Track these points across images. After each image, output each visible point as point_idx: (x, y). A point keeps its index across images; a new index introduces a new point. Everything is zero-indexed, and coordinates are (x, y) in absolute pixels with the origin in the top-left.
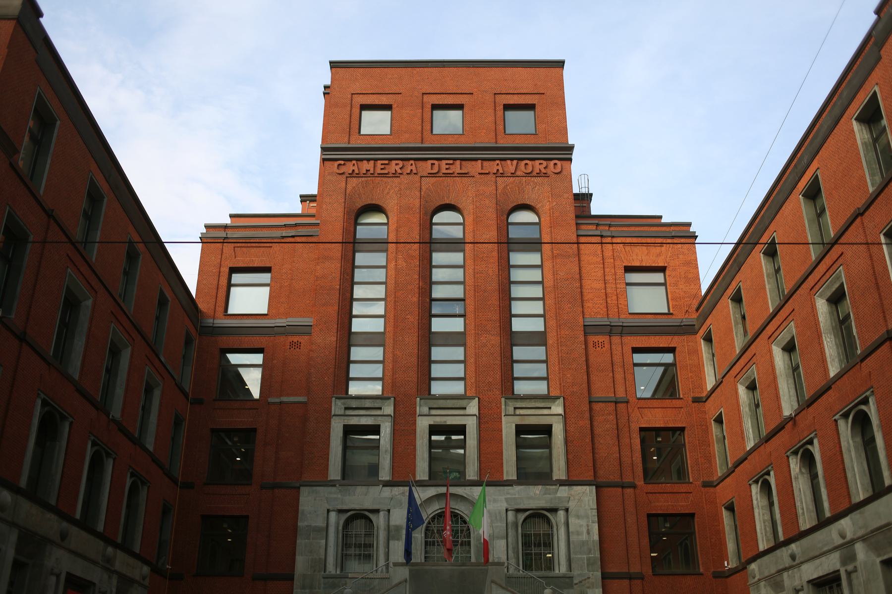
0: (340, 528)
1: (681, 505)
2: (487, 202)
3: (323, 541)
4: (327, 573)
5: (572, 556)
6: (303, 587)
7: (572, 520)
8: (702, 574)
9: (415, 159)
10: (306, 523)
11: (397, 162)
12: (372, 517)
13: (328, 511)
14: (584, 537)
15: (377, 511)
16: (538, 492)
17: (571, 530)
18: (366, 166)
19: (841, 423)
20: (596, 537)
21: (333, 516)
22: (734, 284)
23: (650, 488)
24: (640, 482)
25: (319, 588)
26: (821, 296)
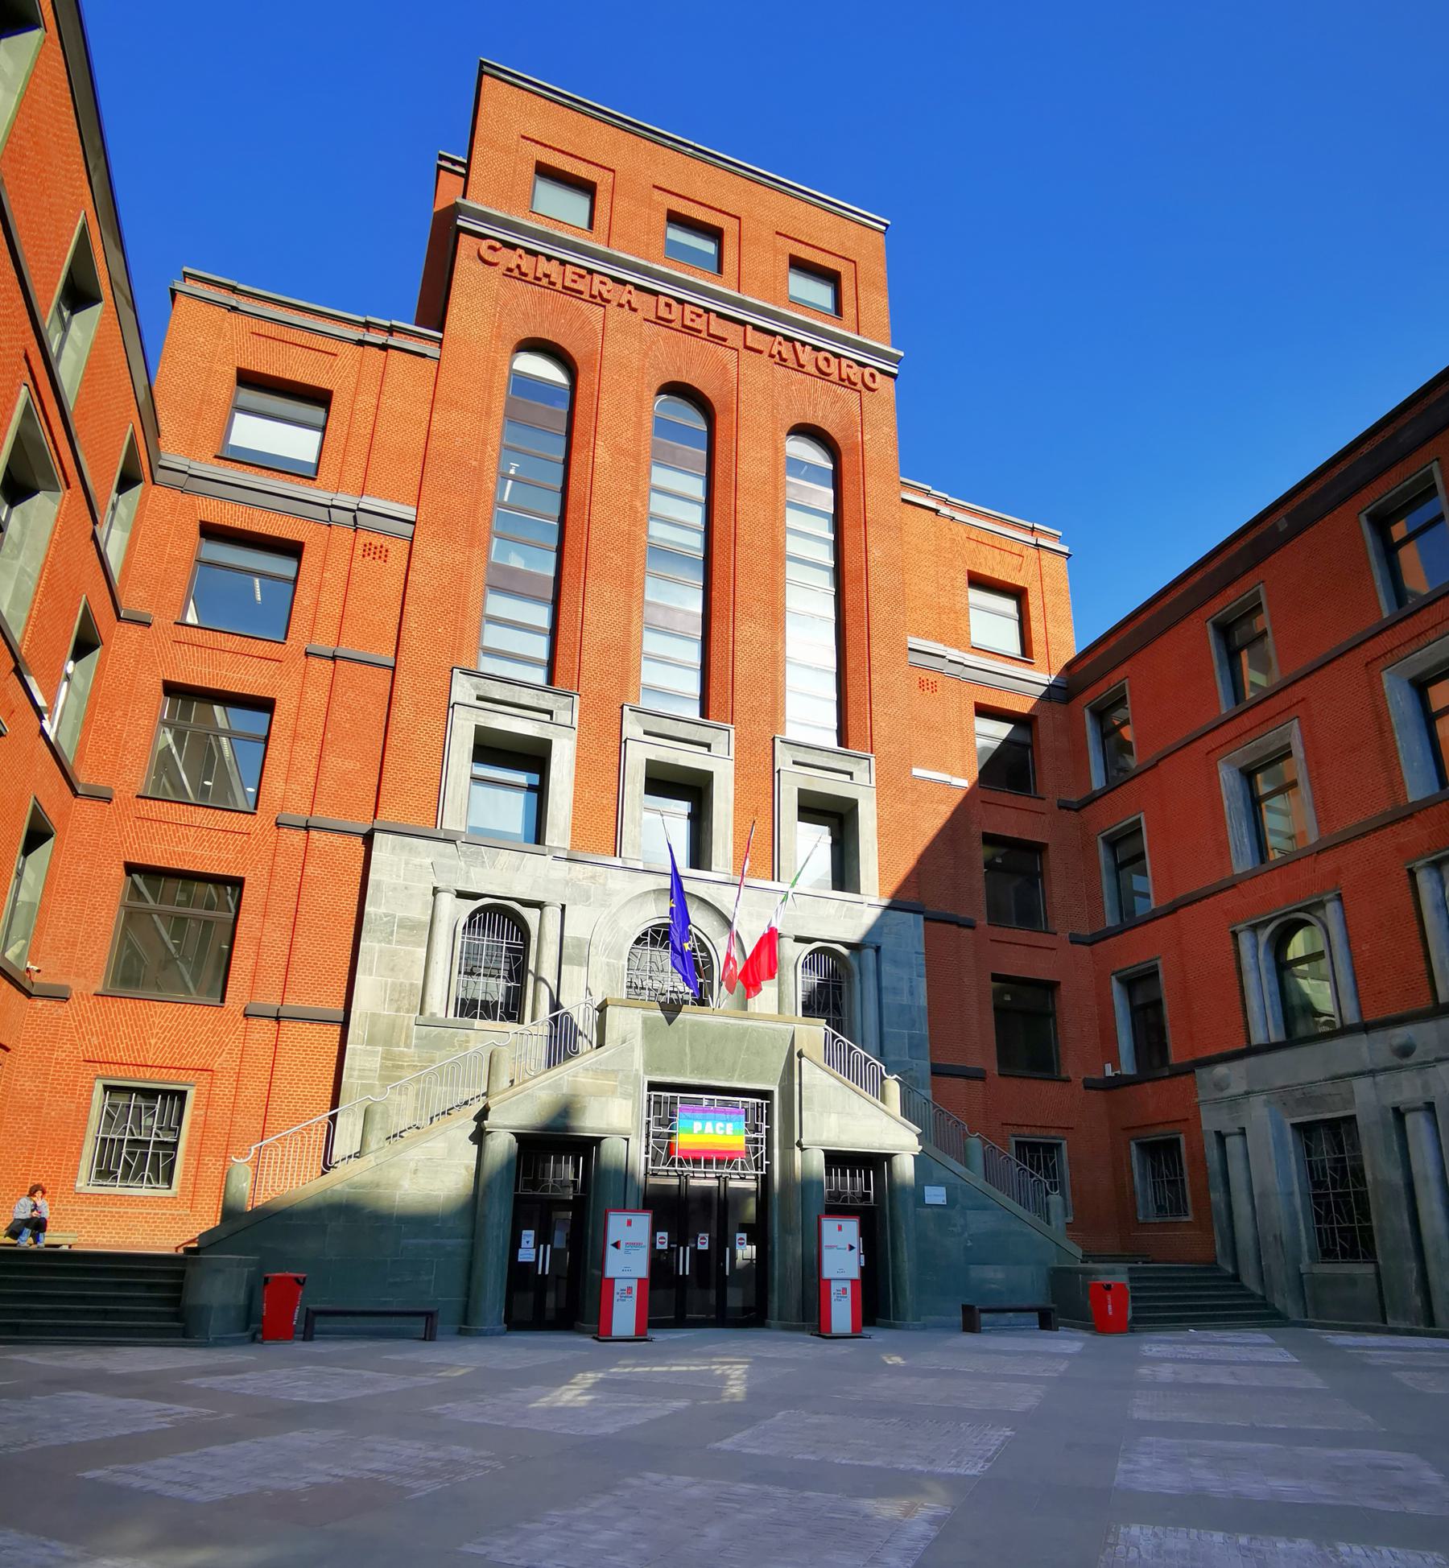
0: (460, 929)
1: (1039, 968)
2: (759, 398)
3: (422, 952)
4: (427, 1013)
5: (886, 1029)
6: (371, 1041)
7: (886, 968)
8: (1068, 1080)
9: (638, 287)
10: (382, 910)
11: (605, 279)
12: (531, 916)
13: (435, 891)
14: (905, 1000)
15: (539, 905)
16: (832, 911)
17: (884, 983)
18: (544, 266)
19: (1245, 940)
20: (923, 1001)
21: (447, 901)
22: (1116, 676)
23: (997, 932)
24: (982, 922)
25: (407, 1046)
26: (1228, 762)
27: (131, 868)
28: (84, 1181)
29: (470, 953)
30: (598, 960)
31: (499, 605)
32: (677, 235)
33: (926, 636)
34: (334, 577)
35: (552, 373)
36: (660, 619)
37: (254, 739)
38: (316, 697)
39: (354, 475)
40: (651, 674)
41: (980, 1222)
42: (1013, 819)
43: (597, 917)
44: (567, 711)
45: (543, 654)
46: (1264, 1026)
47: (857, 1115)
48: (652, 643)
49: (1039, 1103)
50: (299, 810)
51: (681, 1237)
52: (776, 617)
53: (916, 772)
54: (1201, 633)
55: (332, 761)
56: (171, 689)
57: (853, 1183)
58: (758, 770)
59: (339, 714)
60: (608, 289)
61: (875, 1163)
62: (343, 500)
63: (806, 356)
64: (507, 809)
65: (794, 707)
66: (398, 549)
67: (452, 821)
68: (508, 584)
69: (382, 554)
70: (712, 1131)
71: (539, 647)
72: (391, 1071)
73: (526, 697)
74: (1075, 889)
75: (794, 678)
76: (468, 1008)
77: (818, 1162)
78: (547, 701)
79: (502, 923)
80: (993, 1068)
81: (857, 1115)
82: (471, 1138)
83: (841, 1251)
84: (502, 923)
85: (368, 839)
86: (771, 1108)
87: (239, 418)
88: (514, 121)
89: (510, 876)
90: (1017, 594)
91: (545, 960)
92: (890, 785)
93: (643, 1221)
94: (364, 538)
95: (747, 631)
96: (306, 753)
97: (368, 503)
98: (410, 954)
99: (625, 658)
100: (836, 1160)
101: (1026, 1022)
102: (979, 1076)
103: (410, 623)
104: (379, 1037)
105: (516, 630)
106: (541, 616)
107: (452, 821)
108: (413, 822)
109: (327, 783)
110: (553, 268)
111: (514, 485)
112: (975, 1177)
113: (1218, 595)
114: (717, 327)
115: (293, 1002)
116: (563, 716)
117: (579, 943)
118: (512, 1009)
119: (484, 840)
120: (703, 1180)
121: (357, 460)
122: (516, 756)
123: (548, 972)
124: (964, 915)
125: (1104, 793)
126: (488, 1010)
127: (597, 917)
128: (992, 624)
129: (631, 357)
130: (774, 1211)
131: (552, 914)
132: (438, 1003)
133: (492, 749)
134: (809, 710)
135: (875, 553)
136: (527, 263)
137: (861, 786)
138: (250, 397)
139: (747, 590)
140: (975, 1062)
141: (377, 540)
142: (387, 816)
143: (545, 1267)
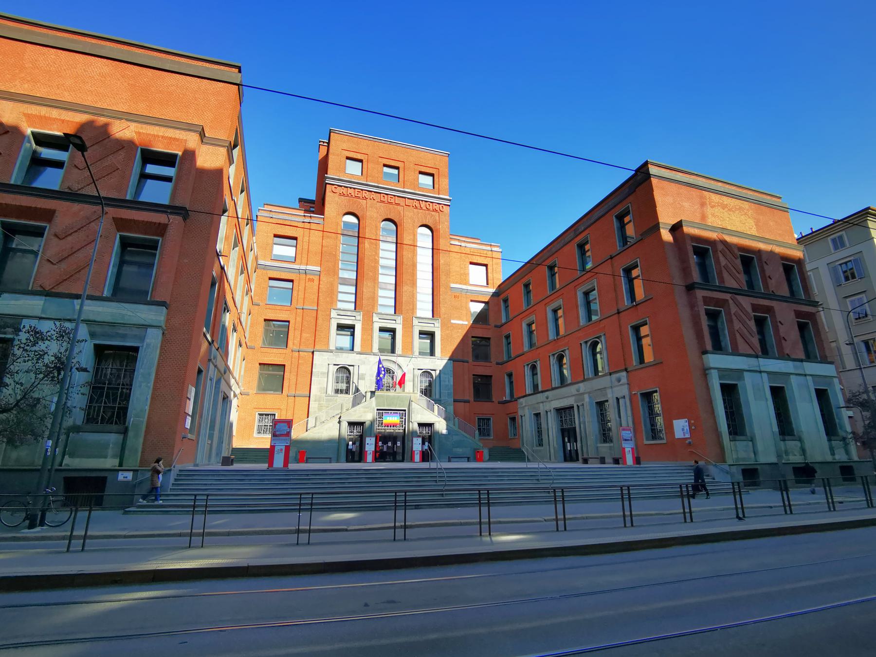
12: (351, 368)
18: (350, 191)
23: (476, 363)
24: (471, 361)
27: (260, 364)
28: (255, 435)
29: (337, 378)
30: (367, 378)
31: (342, 288)
32: (386, 169)
33: (456, 283)
34: (302, 288)
35: (354, 220)
36: (383, 286)
37: (411, 527)
38: (299, 319)
39: (304, 260)
40: (381, 301)
41: (455, 438)
42: (480, 333)
43: (365, 372)
44: (359, 316)
45: (354, 300)
46: (556, 382)
47: (427, 414)
48: (381, 293)
49: (485, 408)
50: (296, 348)
51: (385, 442)
52: (414, 283)
53: (453, 321)
54: (573, 248)
55: (304, 335)
56: (265, 320)
57: (425, 431)
58: (408, 326)
59: (305, 323)
60: (367, 195)
61: (430, 425)
62: (303, 267)
63: (423, 204)
64: (344, 340)
65: (419, 305)
66: (316, 278)
67: (332, 347)
68: (345, 282)
69: (312, 280)
70: (389, 419)
71: (352, 298)
72: (320, 408)
73: (349, 313)
74: (497, 351)
75: (419, 297)
76: (337, 391)
77: (416, 427)
78: (354, 314)
79: (345, 370)
80: (472, 399)
81: (427, 414)
82: (422, 392)
83: (417, 445)
84: (345, 370)
85: (313, 353)
86: (404, 413)
87: (275, 246)
88: (340, 144)
89: (345, 359)
90: (486, 265)
91: (354, 378)
92: (445, 326)
93: (373, 439)
94: (308, 277)
95: (405, 289)
96: (298, 333)
97: (309, 267)
98: (324, 380)
99: (374, 298)
100: (420, 425)
101: (482, 387)
102: (468, 402)
103: (321, 298)
104: (318, 400)
105: (346, 295)
106: (352, 289)
107: (332, 347)
108: (324, 348)
109: (303, 340)
110: (351, 191)
111: (346, 248)
112: (456, 428)
113: (545, 261)
114: (398, 200)
115: (298, 393)
116: (358, 318)
117: (363, 375)
118: (347, 391)
119: (340, 349)
120: (390, 430)
121: (305, 256)
122: (347, 328)
123: (355, 381)
124: (466, 359)
125: (506, 323)
126: (342, 392)
127: (365, 372)
128: (477, 275)
129: (373, 211)
130: (405, 438)
131: (356, 368)
132: (330, 391)
133: (341, 327)
134: (424, 307)
135: (442, 261)
136: (345, 191)
137: (436, 328)
138: (277, 240)
139: (405, 277)
140: (467, 398)
141: (311, 277)
142: (317, 348)
143: (354, 450)
